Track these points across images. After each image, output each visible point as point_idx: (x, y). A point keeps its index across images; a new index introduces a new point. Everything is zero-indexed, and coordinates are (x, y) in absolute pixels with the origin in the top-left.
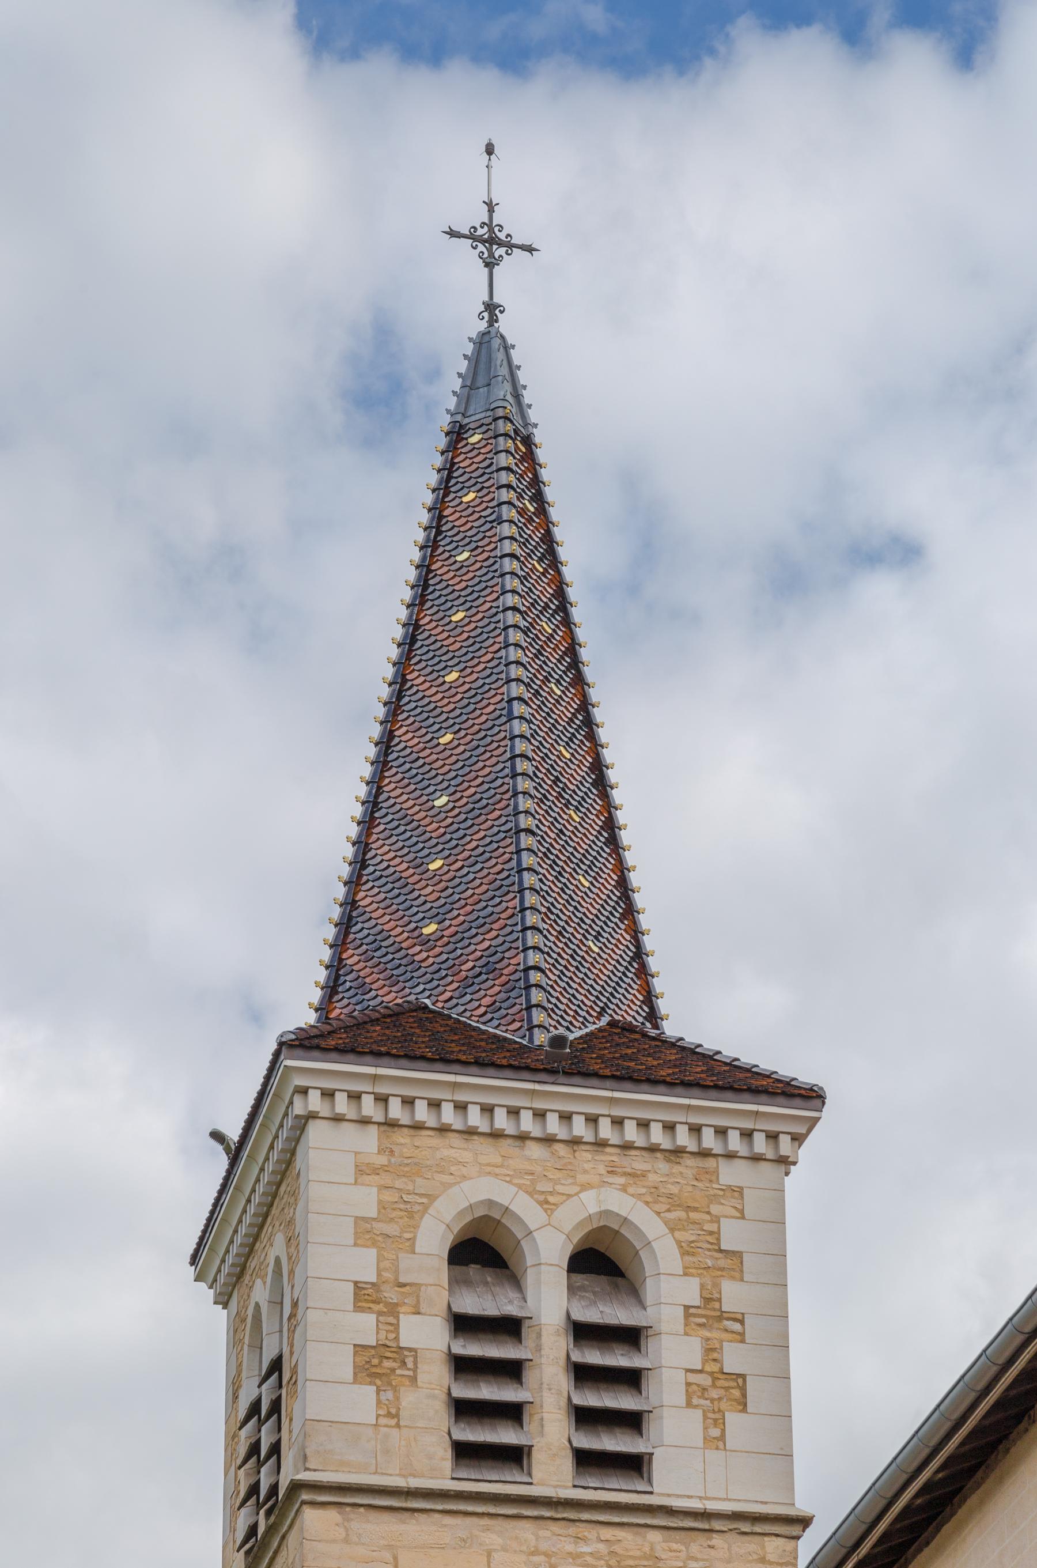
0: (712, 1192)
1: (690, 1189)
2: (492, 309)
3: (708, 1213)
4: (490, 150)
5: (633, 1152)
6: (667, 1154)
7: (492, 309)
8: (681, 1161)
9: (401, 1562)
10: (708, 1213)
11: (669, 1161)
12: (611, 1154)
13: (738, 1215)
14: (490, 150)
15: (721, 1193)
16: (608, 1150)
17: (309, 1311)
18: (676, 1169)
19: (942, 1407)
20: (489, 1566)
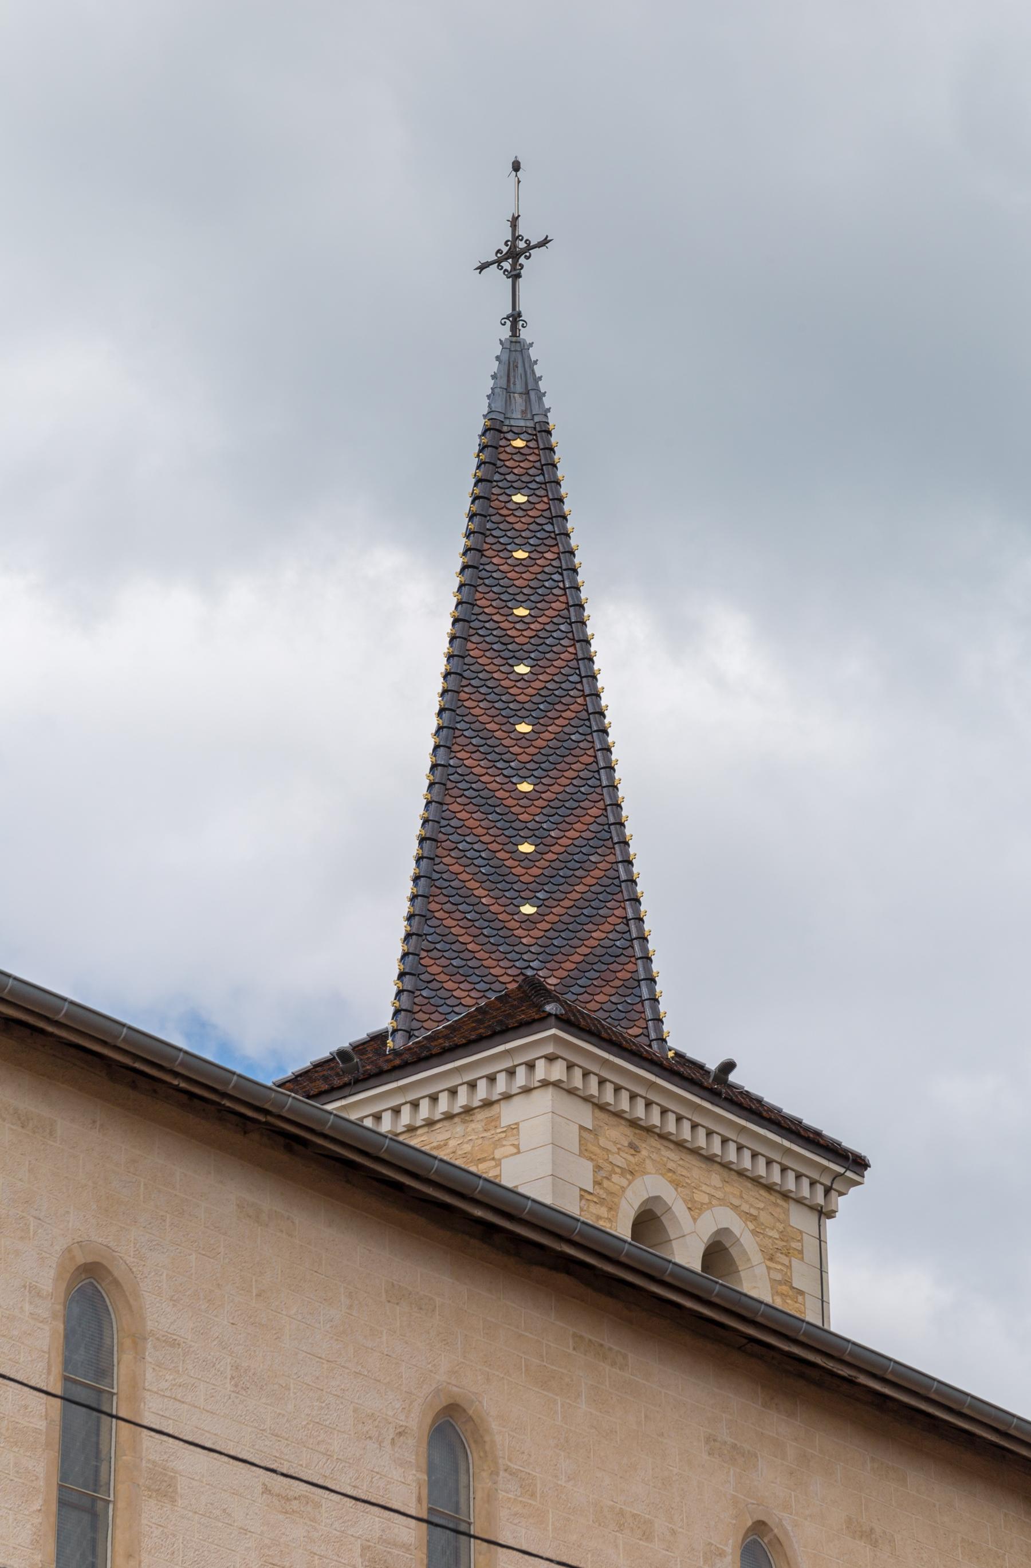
0: (496, 1138)
1: (480, 1141)
2: (515, 319)
3: (493, 1159)
4: (516, 167)
5: (438, 1126)
6: (463, 1116)
7: (515, 319)
8: (473, 1117)
9: (510, 1513)
10: (493, 1159)
11: (464, 1122)
12: (422, 1135)
13: (515, 1151)
14: (516, 167)
15: (503, 1135)
16: (420, 1132)
17: (814, 1217)
18: (473, 1125)
19: (743, 1298)
20: (83, 1511)
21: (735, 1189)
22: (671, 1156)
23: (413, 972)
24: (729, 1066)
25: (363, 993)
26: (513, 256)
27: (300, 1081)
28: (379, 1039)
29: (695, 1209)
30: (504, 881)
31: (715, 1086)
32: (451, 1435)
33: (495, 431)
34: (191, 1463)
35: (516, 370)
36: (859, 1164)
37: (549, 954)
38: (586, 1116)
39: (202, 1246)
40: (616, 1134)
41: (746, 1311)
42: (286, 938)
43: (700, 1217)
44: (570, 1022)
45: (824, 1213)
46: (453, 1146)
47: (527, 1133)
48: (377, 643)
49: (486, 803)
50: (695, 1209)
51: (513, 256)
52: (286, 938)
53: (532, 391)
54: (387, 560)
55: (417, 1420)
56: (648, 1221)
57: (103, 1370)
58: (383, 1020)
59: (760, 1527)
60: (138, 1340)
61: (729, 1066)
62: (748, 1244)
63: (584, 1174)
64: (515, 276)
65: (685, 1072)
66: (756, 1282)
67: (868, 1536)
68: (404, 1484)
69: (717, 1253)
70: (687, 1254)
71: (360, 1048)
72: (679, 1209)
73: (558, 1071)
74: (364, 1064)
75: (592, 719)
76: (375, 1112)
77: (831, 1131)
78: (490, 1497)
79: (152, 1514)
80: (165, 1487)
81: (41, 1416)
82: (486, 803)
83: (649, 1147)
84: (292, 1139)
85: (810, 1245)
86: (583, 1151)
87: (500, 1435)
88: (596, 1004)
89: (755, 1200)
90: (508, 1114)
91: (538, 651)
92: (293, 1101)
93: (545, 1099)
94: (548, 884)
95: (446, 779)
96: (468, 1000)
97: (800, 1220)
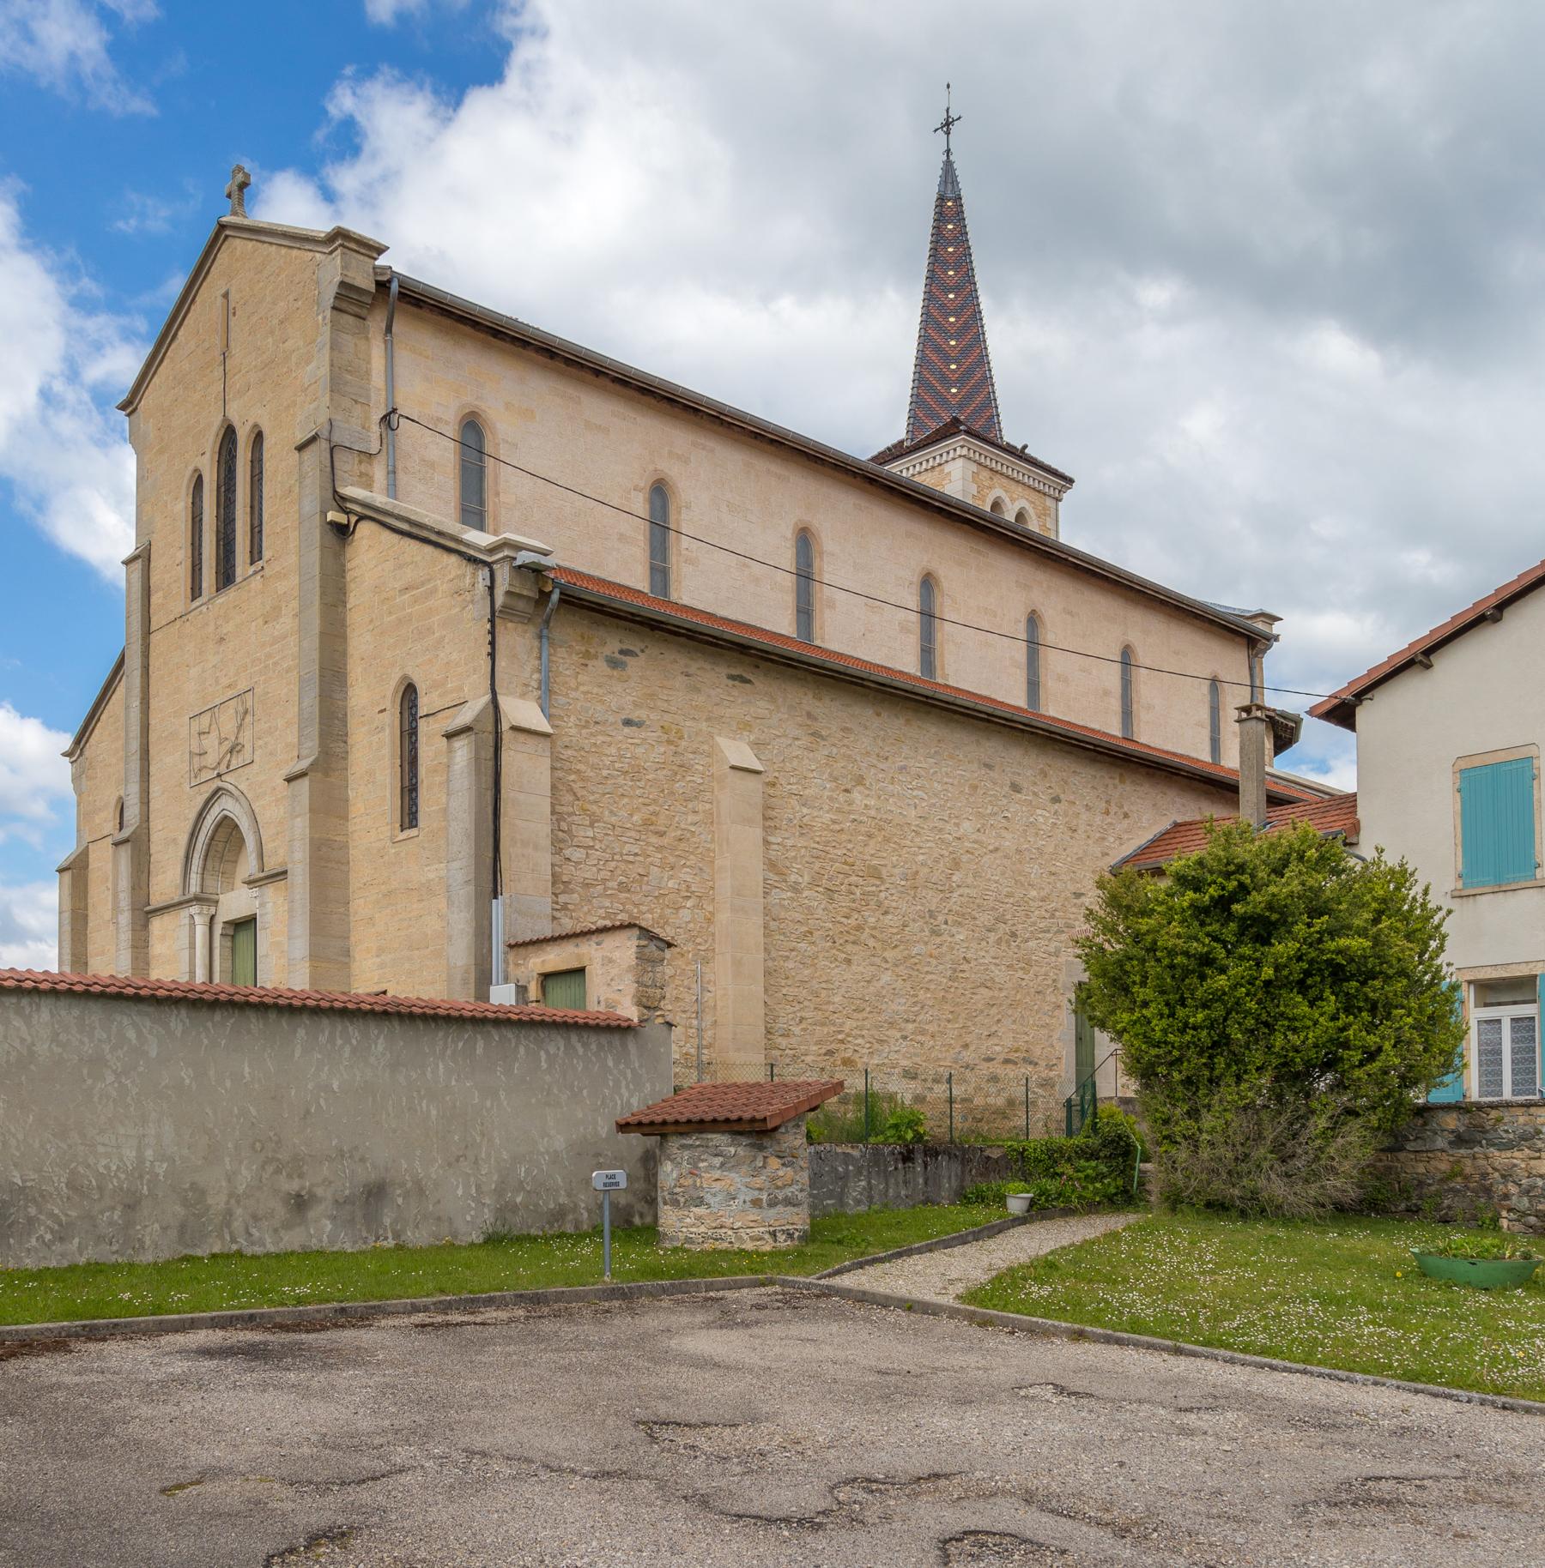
2: (948, 151)
7: (948, 151)
21: (1028, 492)
22: (1004, 481)
23: (917, 402)
24: (1025, 447)
25: (897, 430)
26: (947, 124)
27: (874, 459)
28: (902, 442)
29: (1013, 500)
30: (945, 380)
31: (1020, 454)
32: (928, 584)
33: (941, 199)
34: (841, 596)
35: (949, 173)
36: (1071, 481)
37: (961, 406)
38: (974, 467)
39: (844, 521)
40: (985, 474)
41: (1029, 536)
42: (864, 406)
43: (1014, 504)
44: (968, 433)
45: (1058, 500)
46: (928, 480)
47: (953, 474)
48: (891, 325)
49: (938, 349)
50: (1013, 500)
51: (947, 124)
52: (864, 406)
53: (955, 182)
54: (892, 295)
55: (917, 579)
56: (996, 505)
57: (810, 565)
58: (902, 435)
59: (1034, 612)
60: (821, 554)
61: (1025, 447)
62: (1031, 513)
63: (974, 489)
64: (948, 133)
65: (1009, 450)
66: (1033, 526)
67: (1070, 613)
68: (913, 602)
69: (1020, 516)
70: (1010, 516)
71: (895, 446)
72: (1007, 500)
73: (964, 451)
74: (896, 452)
75: (983, 360)
76: (900, 469)
77: (1061, 470)
78: (942, 605)
79: (827, 612)
80: (831, 605)
81: (789, 581)
82: (938, 349)
83: (997, 478)
84: (872, 481)
85: (1053, 512)
86: (974, 481)
87: (945, 584)
88: (976, 427)
89: (1034, 496)
90: (947, 468)
91: (957, 289)
92: (874, 466)
93: (960, 462)
94: (961, 381)
95: (922, 362)
96: (934, 425)
97: (1050, 502)
